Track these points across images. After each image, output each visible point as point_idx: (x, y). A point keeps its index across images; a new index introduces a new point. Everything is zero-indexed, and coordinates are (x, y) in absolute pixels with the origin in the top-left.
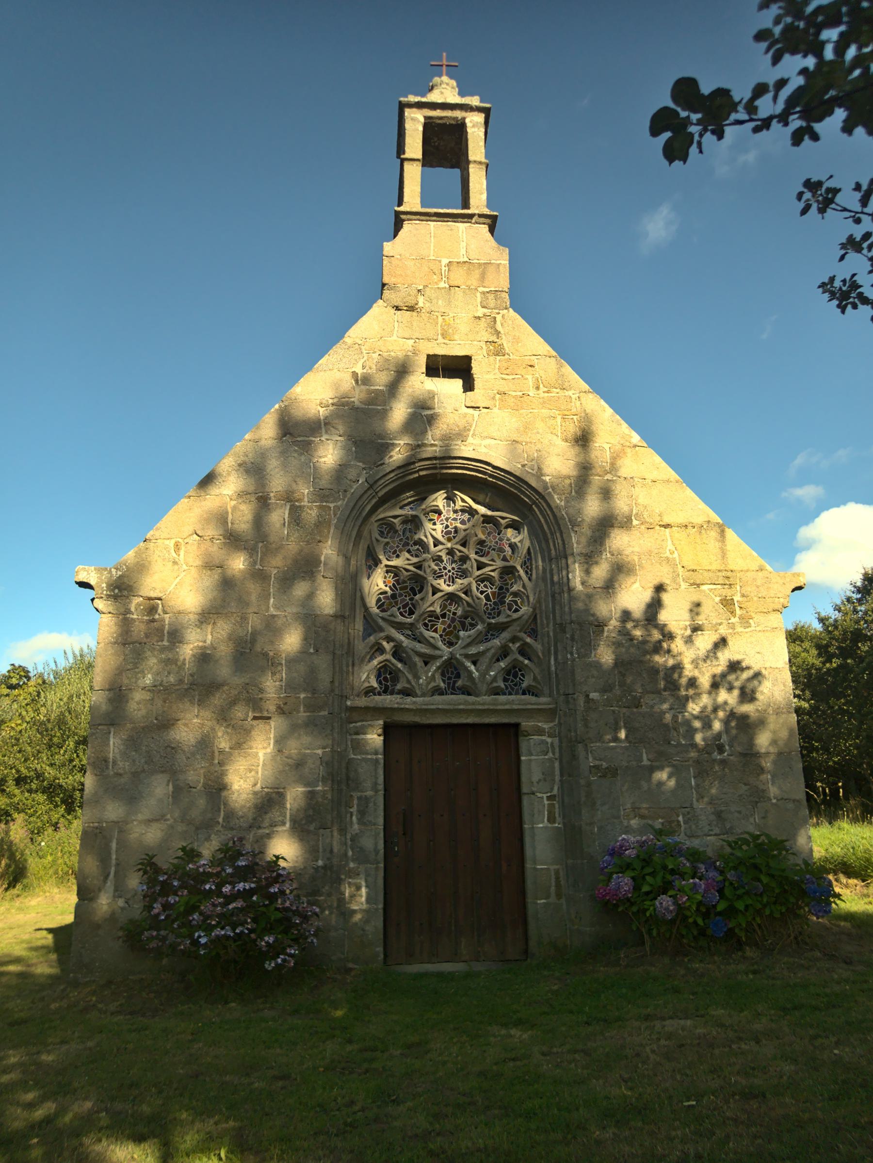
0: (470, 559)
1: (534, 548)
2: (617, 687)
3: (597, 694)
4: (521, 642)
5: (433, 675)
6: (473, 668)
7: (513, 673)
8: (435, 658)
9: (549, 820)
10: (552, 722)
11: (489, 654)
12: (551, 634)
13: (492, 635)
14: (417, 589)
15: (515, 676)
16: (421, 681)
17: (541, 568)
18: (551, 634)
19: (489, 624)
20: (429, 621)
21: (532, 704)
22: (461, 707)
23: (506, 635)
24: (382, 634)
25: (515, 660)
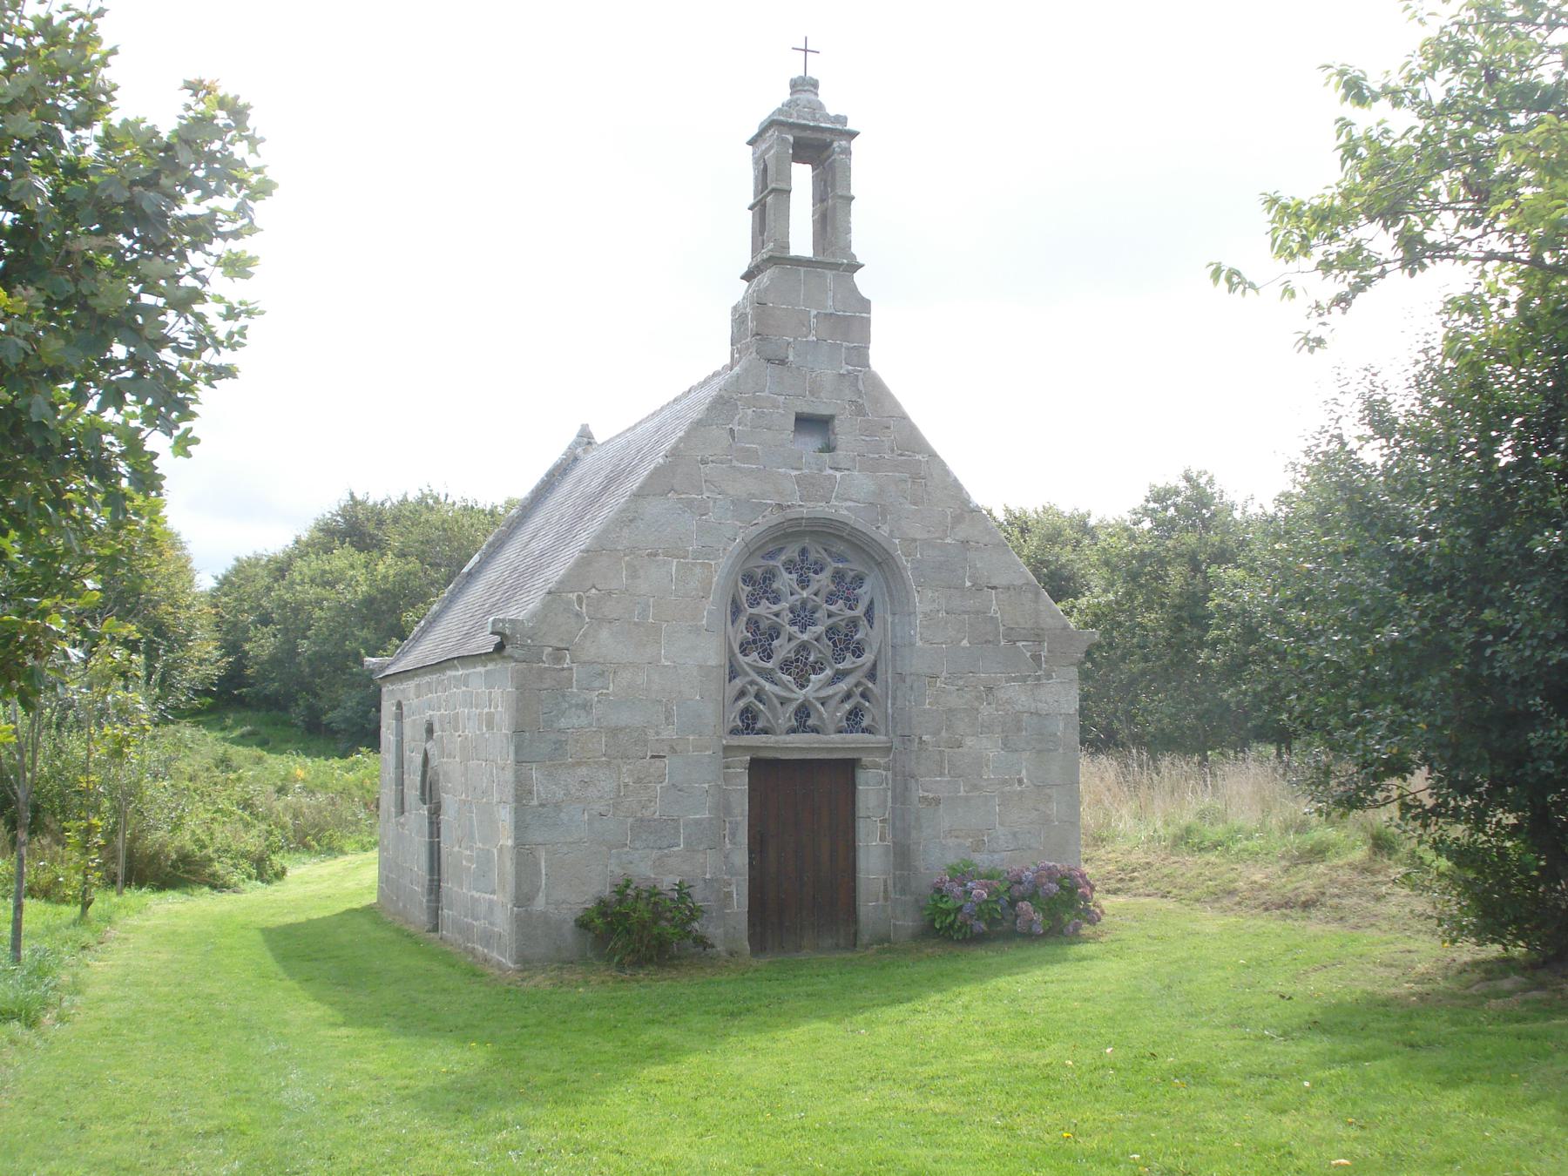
7: (855, 713)
8: (790, 700)
11: (837, 698)
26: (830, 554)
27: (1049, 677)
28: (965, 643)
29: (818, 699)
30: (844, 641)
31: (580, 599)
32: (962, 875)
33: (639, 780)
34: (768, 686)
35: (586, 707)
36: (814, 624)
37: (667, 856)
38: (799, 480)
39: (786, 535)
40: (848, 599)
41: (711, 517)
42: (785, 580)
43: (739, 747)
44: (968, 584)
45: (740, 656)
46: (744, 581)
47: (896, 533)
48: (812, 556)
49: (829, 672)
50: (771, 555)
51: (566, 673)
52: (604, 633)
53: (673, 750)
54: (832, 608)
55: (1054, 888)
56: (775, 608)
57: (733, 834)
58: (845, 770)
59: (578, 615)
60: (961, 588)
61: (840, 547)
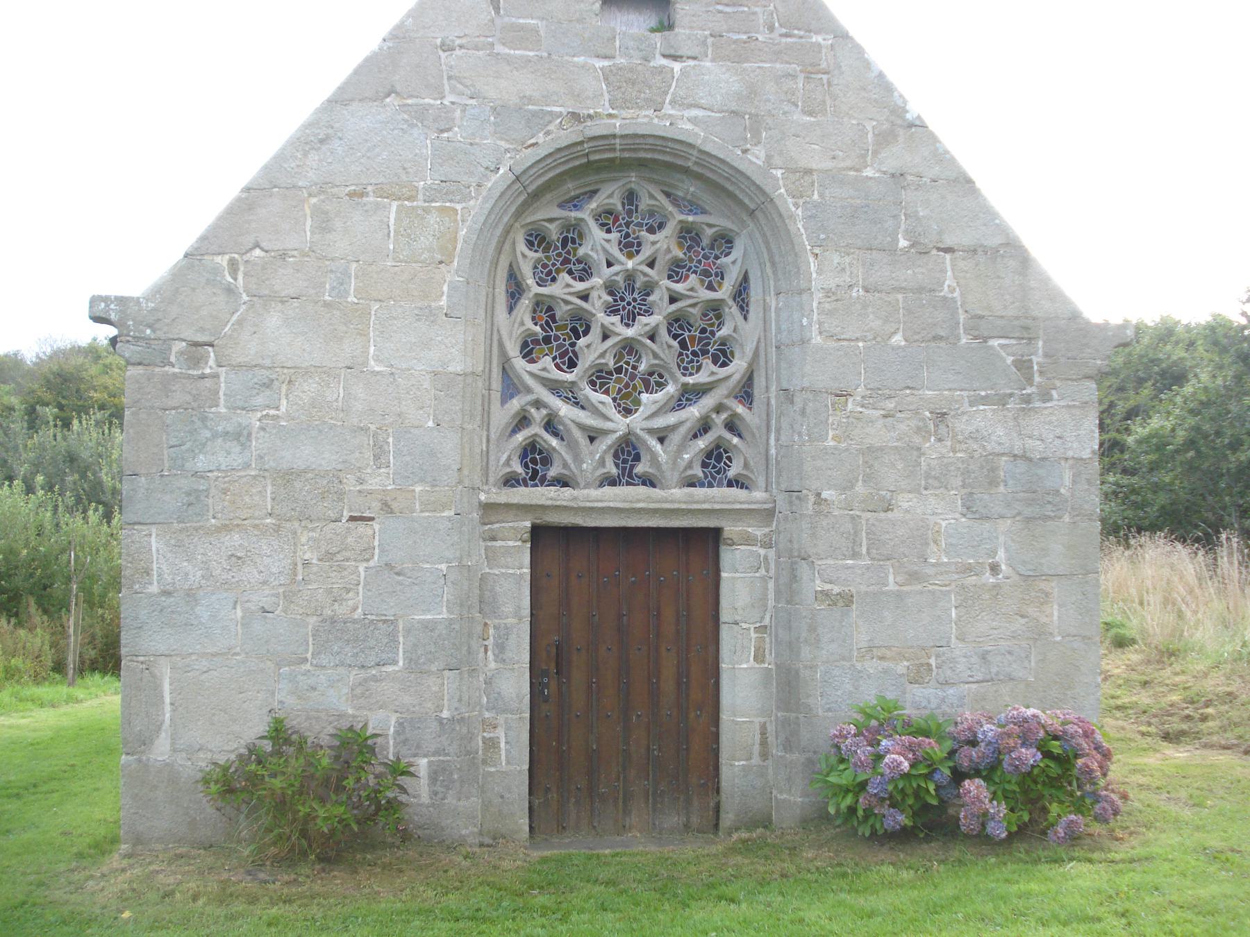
4: (729, 413)
7: (716, 457)
8: (605, 432)
9: (755, 659)
11: (683, 430)
13: (687, 399)
14: (580, 330)
20: (598, 378)
26: (675, 201)
27: (1046, 397)
28: (898, 339)
29: (650, 431)
30: (699, 338)
31: (233, 265)
32: (879, 724)
33: (328, 556)
34: (565, 410)
35: (241, 436)
36: (649, 312)
37: (375, 679)
38: (607, 75)
39: (590, 167)
40: (706, 273)
41: (457, 134)
42: (598, 242)
43: (508, 506)
44: (903, 243)
46: (530, 244)
47: (777, 160)
48: (644, 203)
49: (671, 389)
50: (574, 202)
51: (208, 383)
52: (273, 320)
53: (387, 508)
54: (679, 287)
55: (1030, 756)
56: (580, 286)
57: (501, 647)
58: (701, 544)
59: (230, 291)
60: (892, 250)
61: (690, 188)
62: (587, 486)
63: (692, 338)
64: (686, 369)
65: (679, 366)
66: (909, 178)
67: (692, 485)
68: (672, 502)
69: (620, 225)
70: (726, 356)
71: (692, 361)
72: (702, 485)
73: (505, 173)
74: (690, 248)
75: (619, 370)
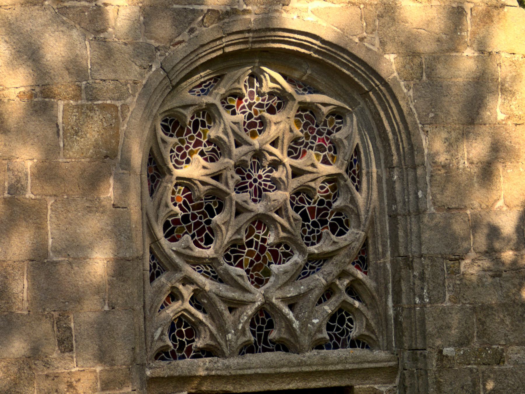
0: (284, 165)
1: (365, 148)
2: (475, 339)
3: (452, 349)
4: (351, 278)
5: (243, 327)
6: (291, 315)
7: (339, 319)
8: (243, 303)
10: (391, 382)
11: (314, 296)
12: (389, 266)
13: (311, 268)
14: (214, 208)
15: (342, 321)
16: (230, 336)
17: (375, 175)
18: (389, 266)
19: (311, 254)
20: (232, 252)
21: (369, 362)
22: (284, 370)
23: (328, 268)
24: (179, 276)
25: (344, 301)
29: (284, 300)
45: (165, 242)
46: (166, 129)
62: (232, 355)
63: (312, 209)
64: (308, 239)
65: (302, 237)
66: (503, 55)
67: (319, 347)
68: (310, 365)
69: (244, 107)
70: (342, 225)
71: (313, 231)
72: (328, 347)
73: (157, 70)
74: (306, 126)
75: (250, 244)
